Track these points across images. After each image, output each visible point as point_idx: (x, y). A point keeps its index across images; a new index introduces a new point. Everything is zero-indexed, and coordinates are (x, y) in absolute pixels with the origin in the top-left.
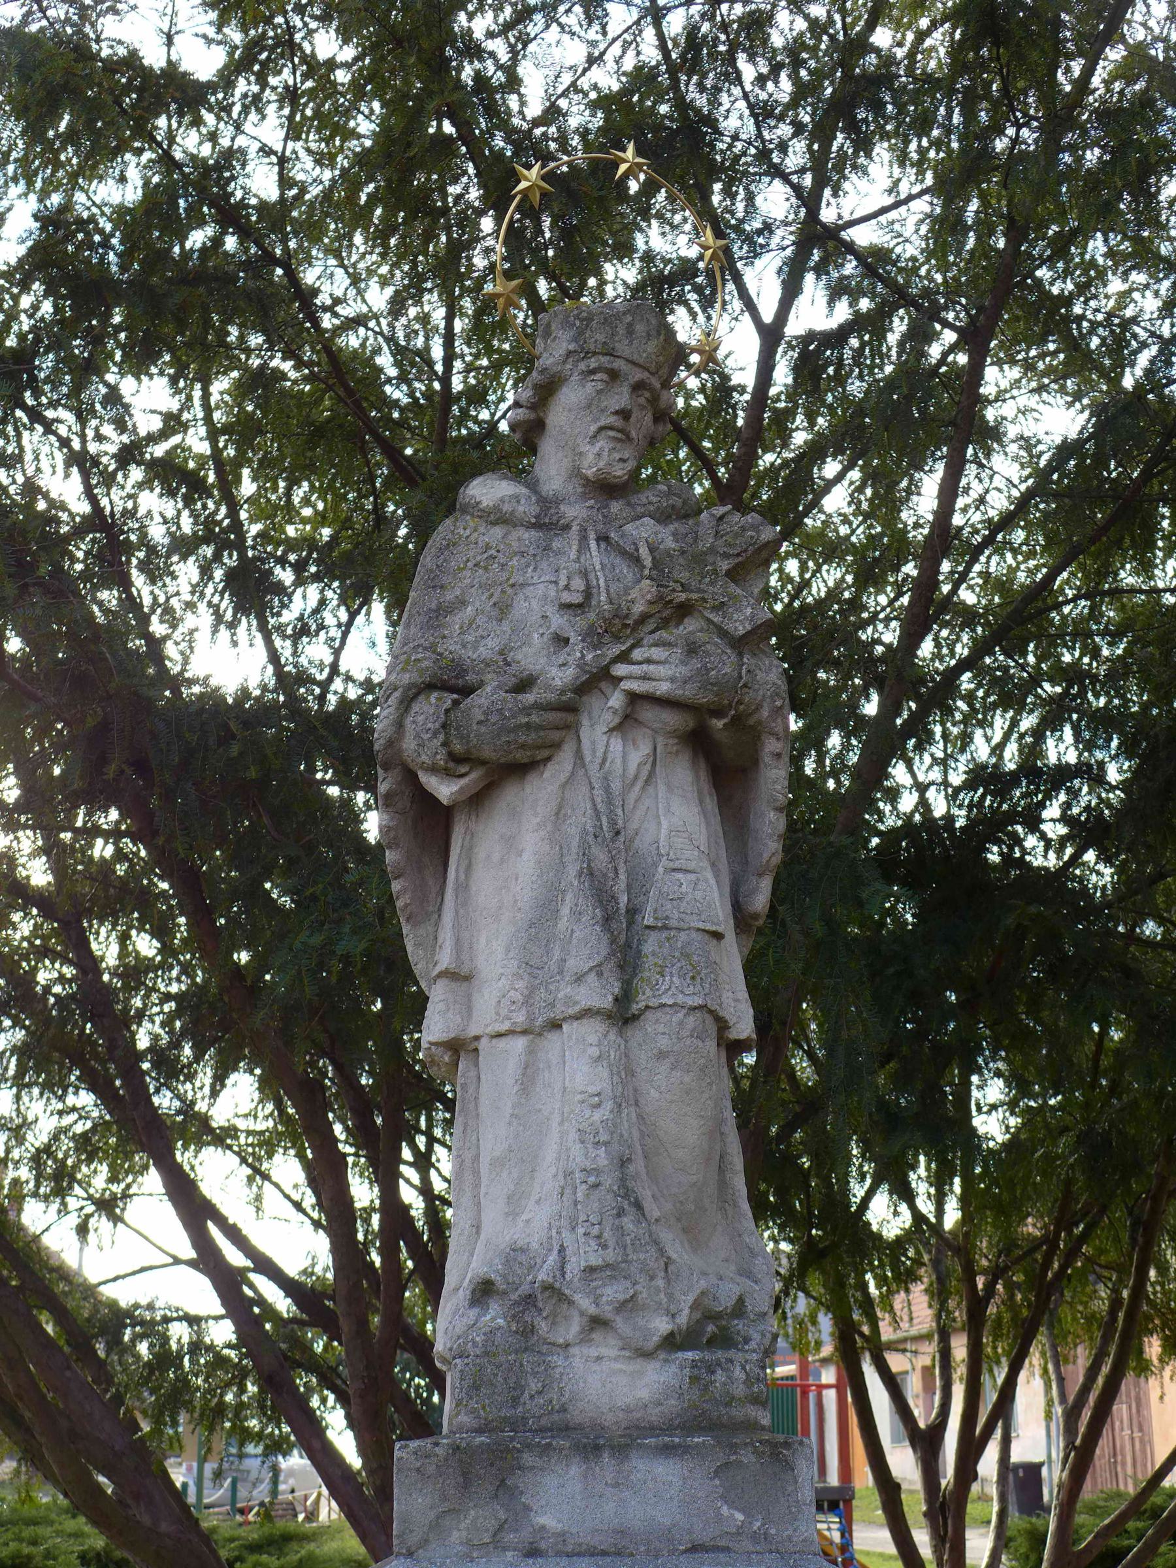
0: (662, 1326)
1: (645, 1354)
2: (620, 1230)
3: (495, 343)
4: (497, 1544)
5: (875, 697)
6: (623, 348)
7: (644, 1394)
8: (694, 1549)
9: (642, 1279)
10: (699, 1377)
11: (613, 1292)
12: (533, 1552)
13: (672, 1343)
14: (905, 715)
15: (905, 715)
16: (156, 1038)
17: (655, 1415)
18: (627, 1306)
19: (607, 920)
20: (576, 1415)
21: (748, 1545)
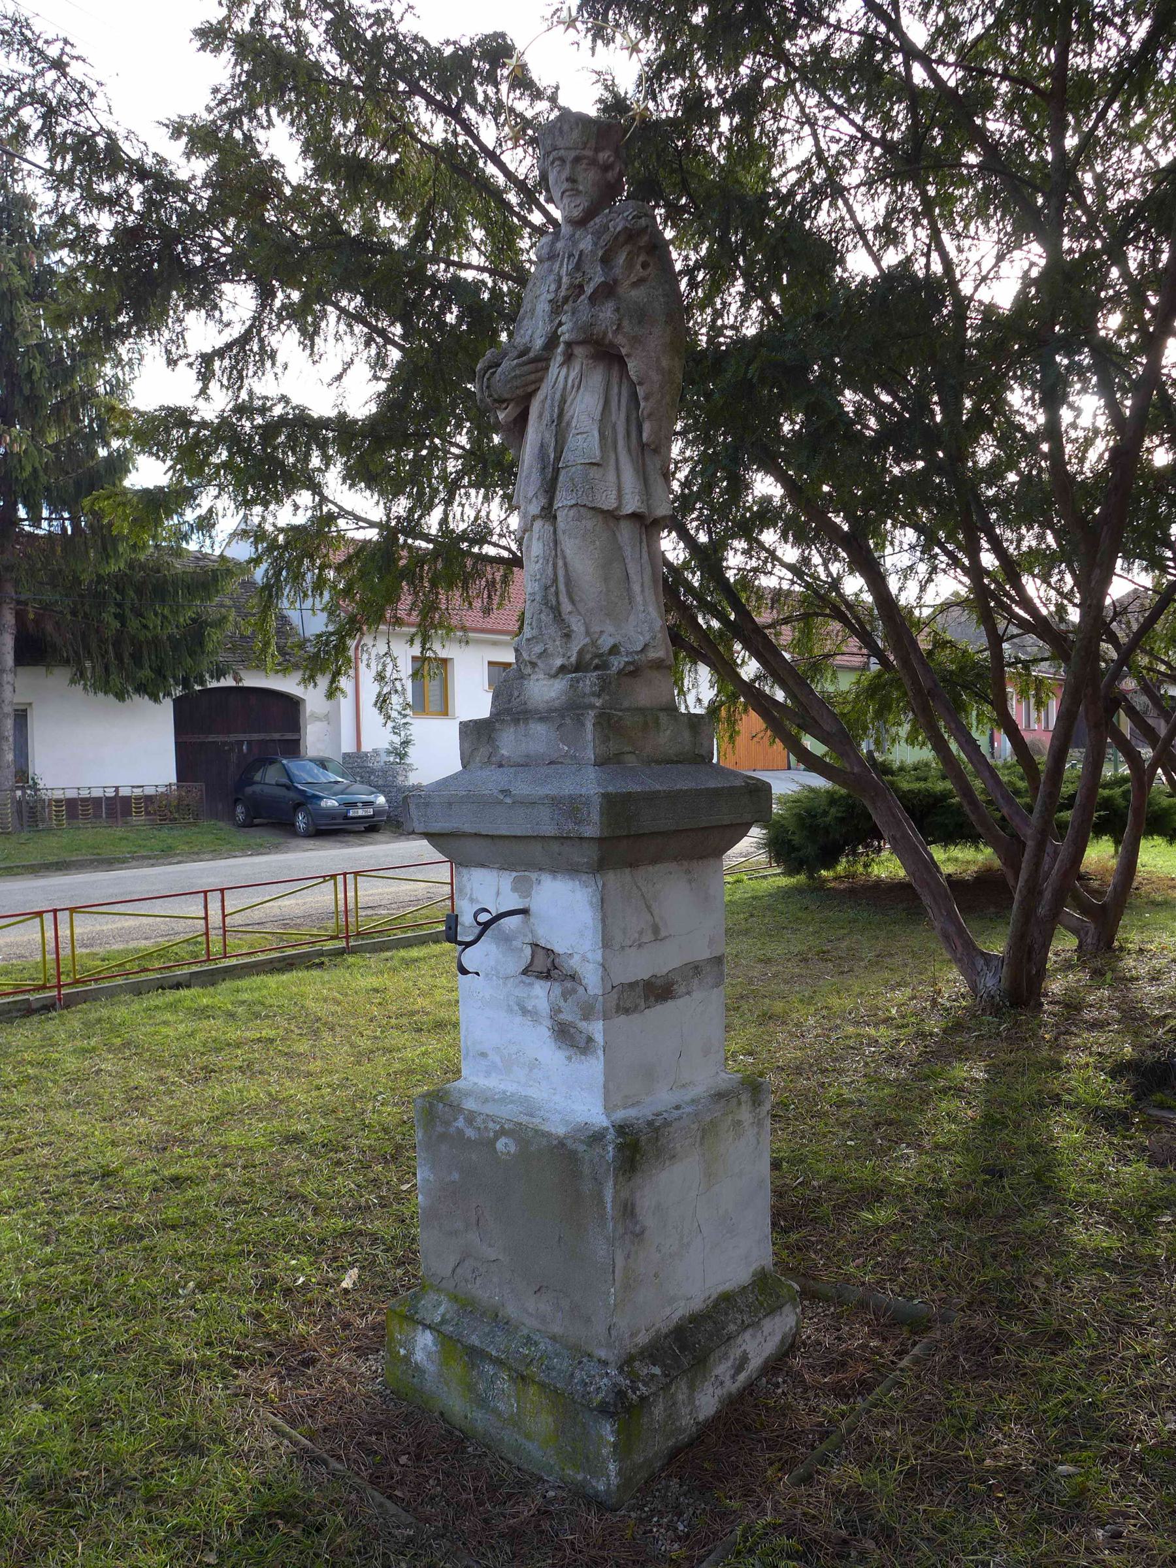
0: (559, 662)
1: (555, 676)
2: (539, 620)
3: (361, 96)
4: (489, 762)
5: (455, 309)
6: (560, 143)
7: (553, 694)
8: (551, 763)
9: (550, 642)
10: (573, 686)
11: (538, 649)
12: (501, 766)
13: (563, 669)
14: (937, 409)
15: (937, 409)
16: (481, 534)
17: (557, 704)
18: (544, 654)
19: (544, 468)
20: (530, 706)
21: (568, 761)
